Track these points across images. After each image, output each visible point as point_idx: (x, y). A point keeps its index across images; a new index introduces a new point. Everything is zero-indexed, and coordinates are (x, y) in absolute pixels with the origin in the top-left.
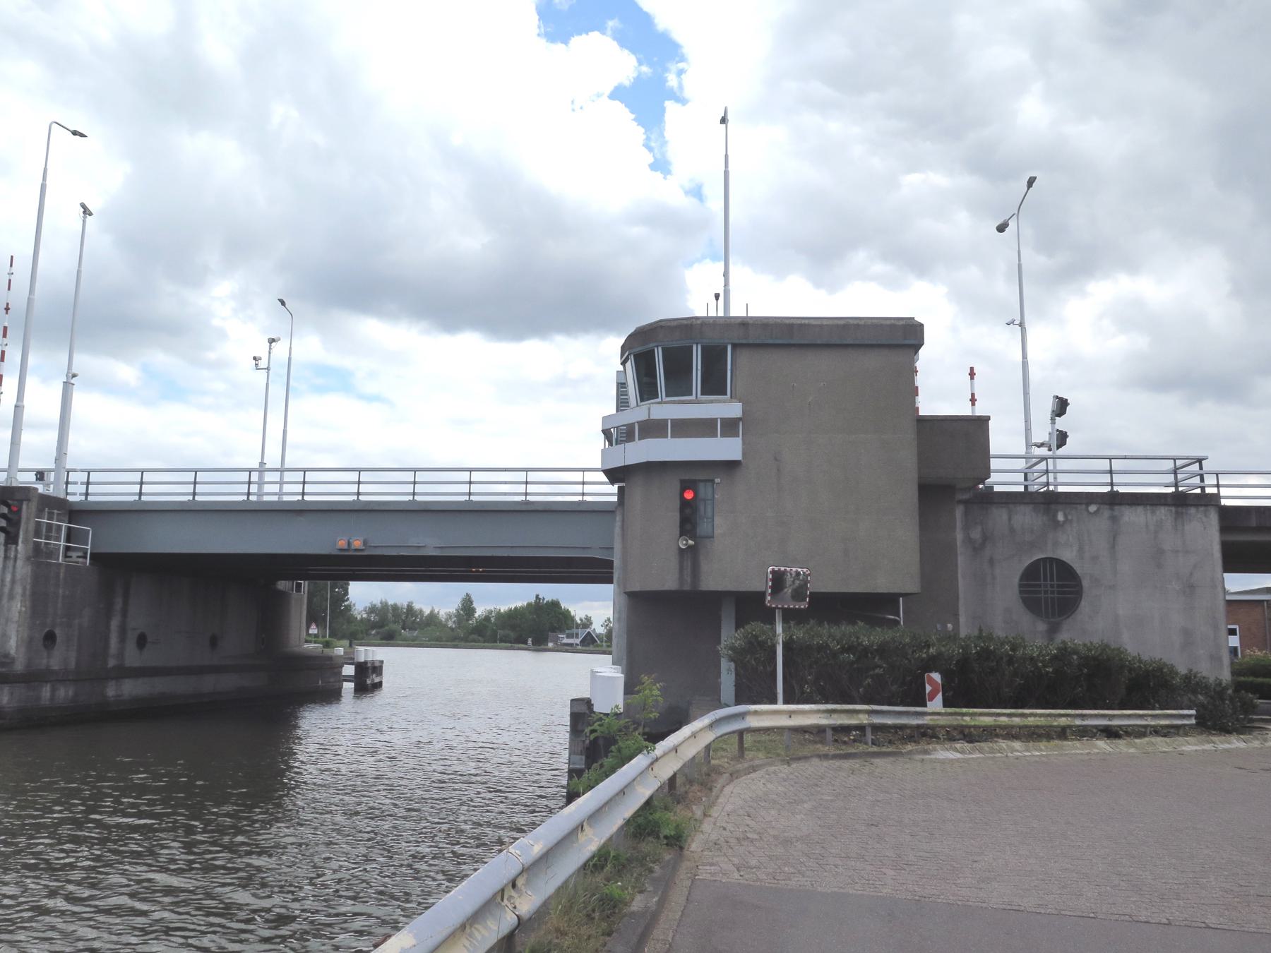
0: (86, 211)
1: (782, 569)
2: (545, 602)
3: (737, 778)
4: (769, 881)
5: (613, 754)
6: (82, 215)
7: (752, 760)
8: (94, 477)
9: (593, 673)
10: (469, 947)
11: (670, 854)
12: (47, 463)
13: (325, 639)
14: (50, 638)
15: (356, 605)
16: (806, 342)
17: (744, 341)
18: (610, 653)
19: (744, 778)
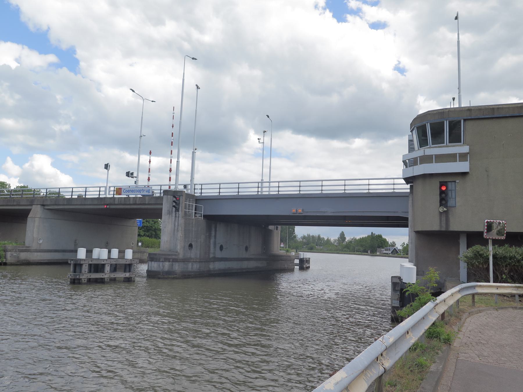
0: (198, 87)
1: (492, 221)
2: (375, 235)
3: (472, 315)
4: (494, 363)
5: (417, 301)
6: (196, 89)
7: (479, 307)
8: (203, 187)
9: (401, 265)
10: (365, 379)
11: (445, 347)
12: (187, 181)
13: (286, 249)
14: (191, 246)
15: (298, 236)
16: (501, 116)
17: (470, 118)
18: (407, 258)
19: (475, 315)
